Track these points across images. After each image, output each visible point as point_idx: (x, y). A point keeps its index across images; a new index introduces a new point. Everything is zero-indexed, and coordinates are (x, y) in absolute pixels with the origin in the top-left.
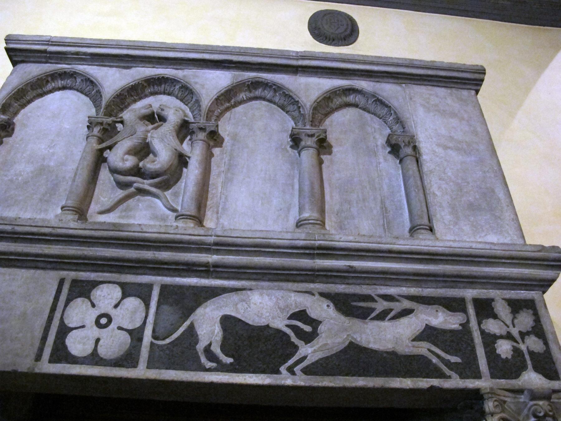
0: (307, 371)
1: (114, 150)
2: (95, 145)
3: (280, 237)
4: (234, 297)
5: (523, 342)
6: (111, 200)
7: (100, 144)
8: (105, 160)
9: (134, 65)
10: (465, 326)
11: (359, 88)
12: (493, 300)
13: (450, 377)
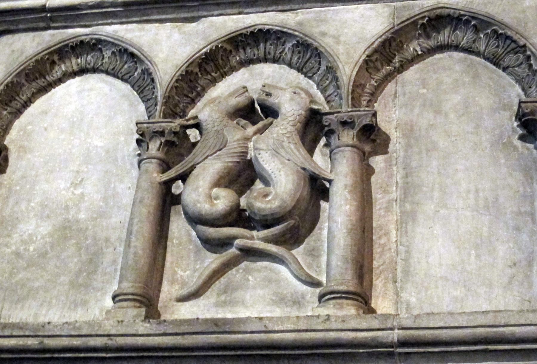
1: (191, 179)
2: (155, 175)
3: (522, 322)
6: (196, 274)
7: (164, 172)
8: (177, 200)
9: (205, 13)
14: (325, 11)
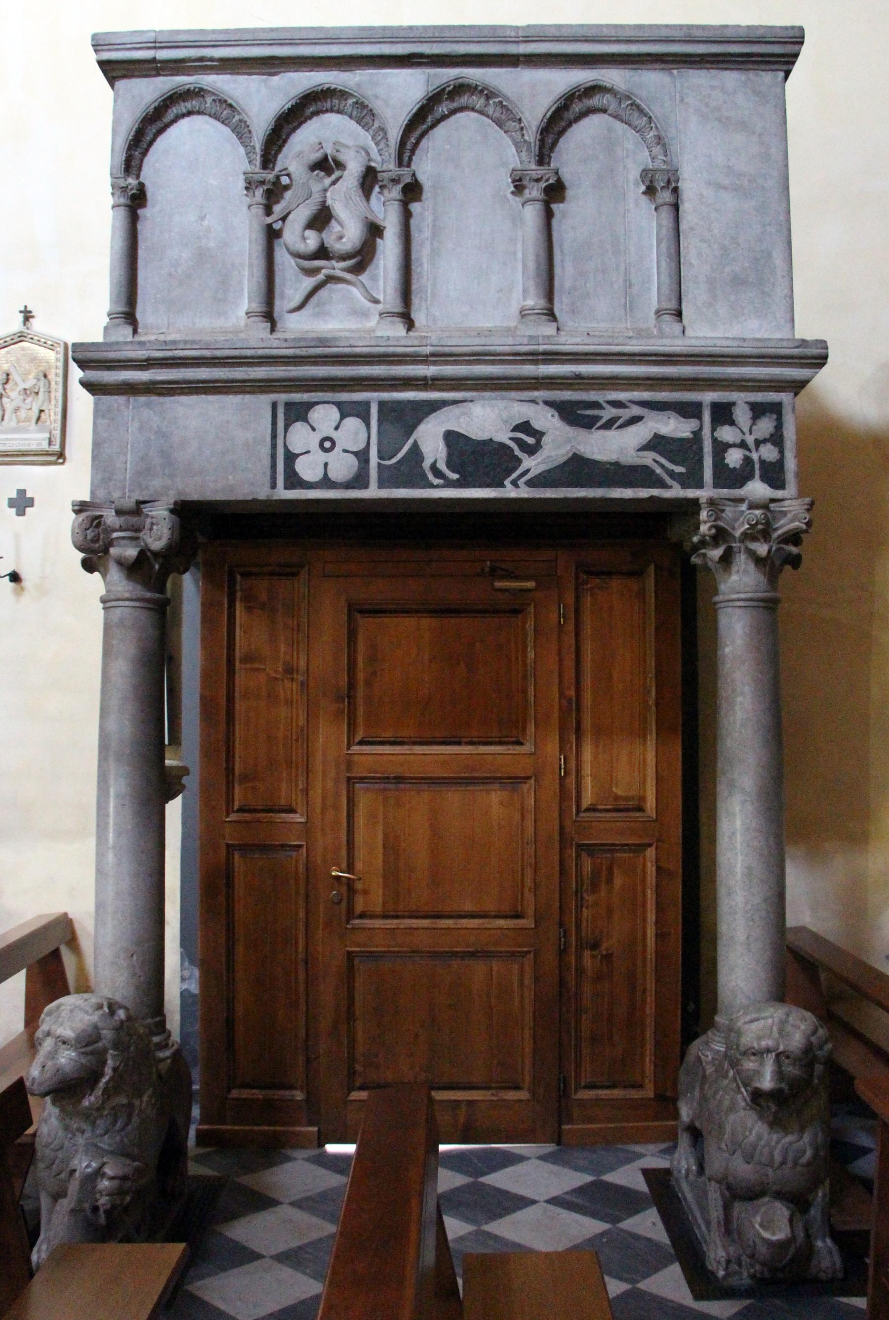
0: (530, 483)
4: (455, 410)
5: (757, 450)
10: (697, 435)
11: (608, 85)
12: (734, 404)
13: (671, 487)
14: (376, 74)
